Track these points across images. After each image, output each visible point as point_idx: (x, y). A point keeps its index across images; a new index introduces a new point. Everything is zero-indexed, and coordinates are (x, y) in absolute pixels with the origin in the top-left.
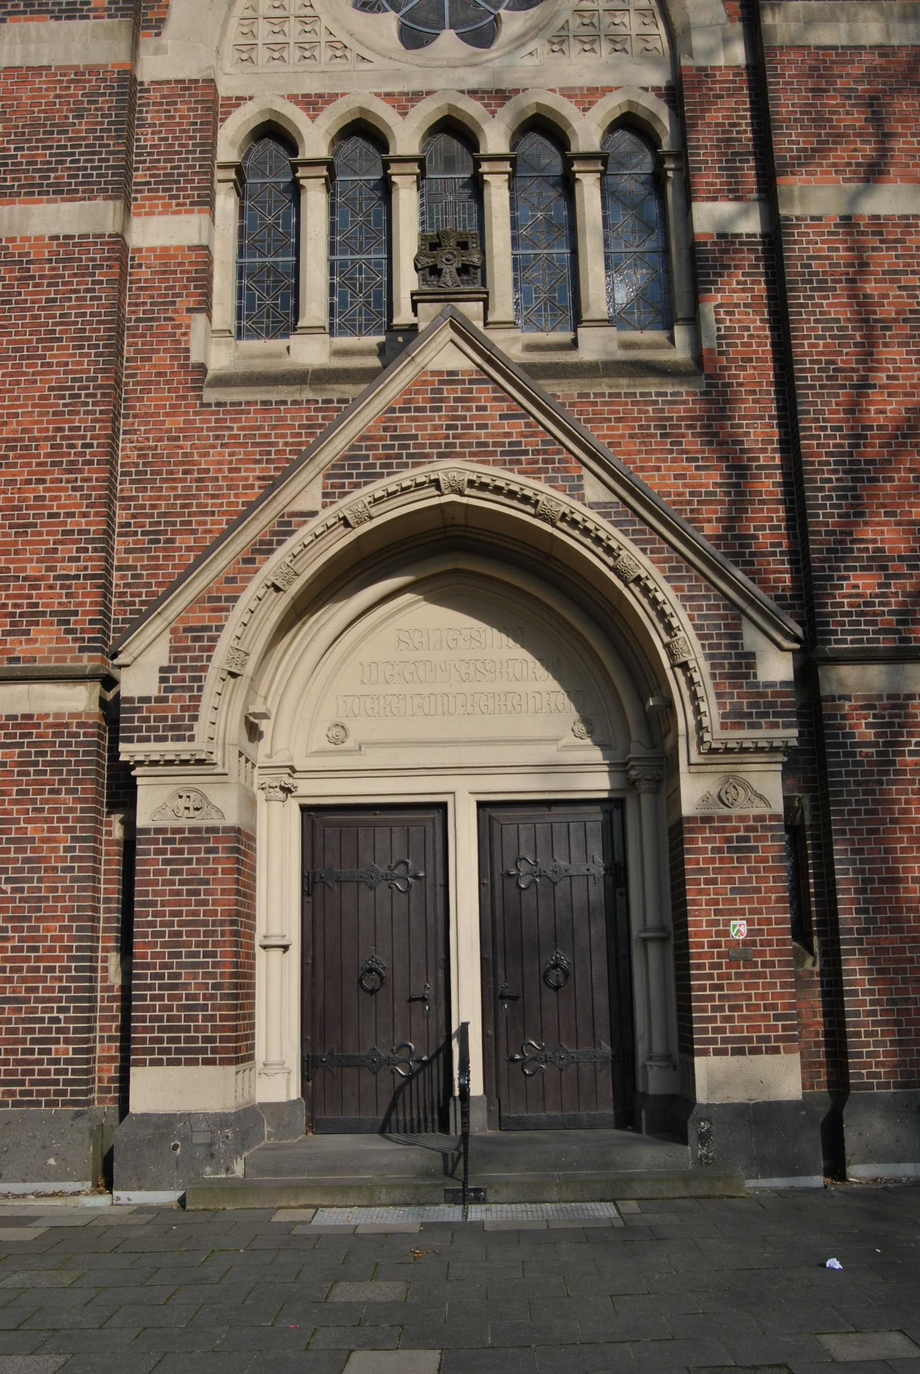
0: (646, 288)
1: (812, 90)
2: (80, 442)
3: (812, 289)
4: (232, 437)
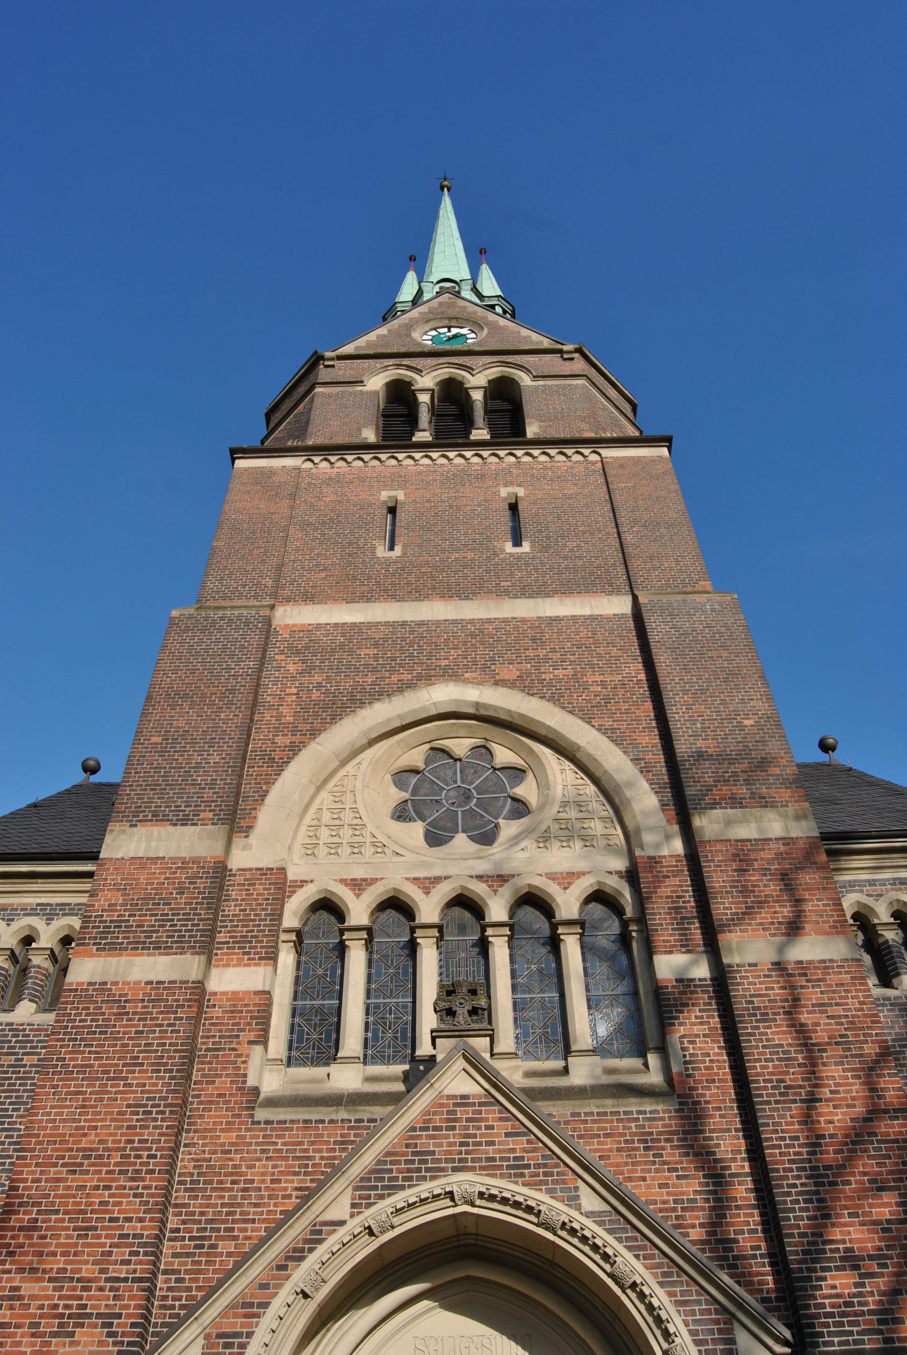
0: (622, 1023)
1: (736, 870)
2: (146, 1153)
3: (757, 1021)
4: (275, 1151)
